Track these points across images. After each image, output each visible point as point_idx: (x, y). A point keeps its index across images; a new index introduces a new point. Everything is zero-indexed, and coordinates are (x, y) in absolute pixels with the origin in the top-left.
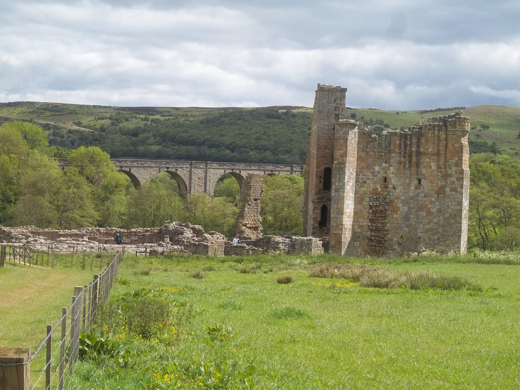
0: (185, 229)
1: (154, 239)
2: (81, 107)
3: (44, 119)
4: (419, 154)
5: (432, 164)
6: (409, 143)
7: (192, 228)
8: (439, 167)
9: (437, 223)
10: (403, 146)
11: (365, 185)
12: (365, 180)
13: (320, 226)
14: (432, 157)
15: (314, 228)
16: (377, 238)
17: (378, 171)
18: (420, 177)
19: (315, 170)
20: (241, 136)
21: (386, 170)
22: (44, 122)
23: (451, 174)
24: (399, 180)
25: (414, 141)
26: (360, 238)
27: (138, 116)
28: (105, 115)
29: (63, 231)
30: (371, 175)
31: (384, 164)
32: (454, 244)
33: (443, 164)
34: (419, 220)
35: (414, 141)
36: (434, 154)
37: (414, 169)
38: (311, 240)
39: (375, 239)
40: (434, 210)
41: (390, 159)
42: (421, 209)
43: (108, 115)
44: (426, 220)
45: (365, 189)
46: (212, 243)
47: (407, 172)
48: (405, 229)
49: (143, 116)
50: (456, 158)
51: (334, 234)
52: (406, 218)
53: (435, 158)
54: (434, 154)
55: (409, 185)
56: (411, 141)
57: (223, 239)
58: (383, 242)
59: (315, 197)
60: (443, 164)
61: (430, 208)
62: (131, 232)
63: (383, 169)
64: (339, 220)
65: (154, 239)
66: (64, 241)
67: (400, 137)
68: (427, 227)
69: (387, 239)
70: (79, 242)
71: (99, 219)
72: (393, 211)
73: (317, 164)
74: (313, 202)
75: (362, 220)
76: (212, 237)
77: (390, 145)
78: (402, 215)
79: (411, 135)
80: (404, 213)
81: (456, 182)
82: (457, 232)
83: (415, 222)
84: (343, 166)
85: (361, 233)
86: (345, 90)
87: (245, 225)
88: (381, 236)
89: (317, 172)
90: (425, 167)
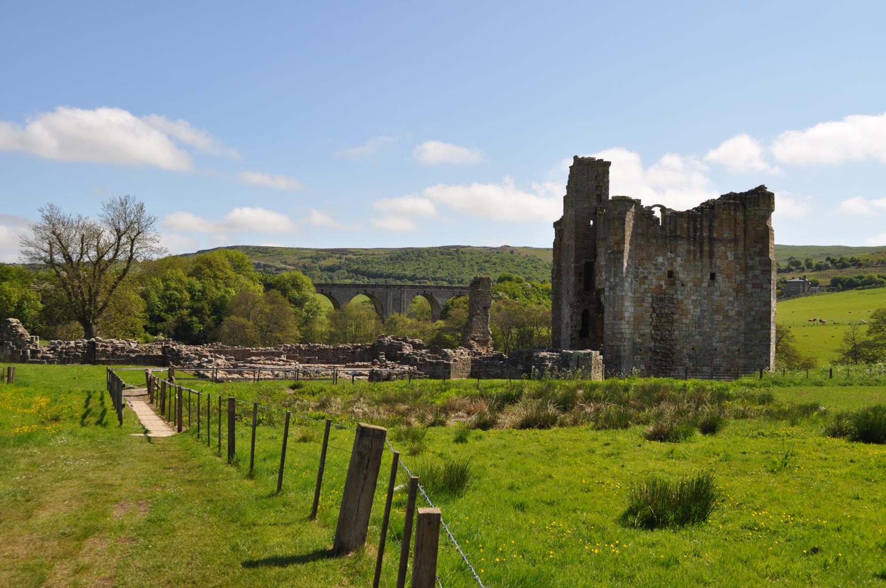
0: (404, 343)
1: (366, 357)
2: (287, 249)
3: (256, 259)
4: (712, 240)
5: (729, 254)
6: (699, 226)
7: (412, 343)
8: (736, 258)
9: (736, 330)
10: (691, 230)
11: (646, 282)
12: (646, 274)
13: (580, 336)
14: (728, 244)
15: (572, 339)
16: (663, 351)
17: (662, 263)
18: (714, 271)
19: (573, 265)
20: (421, 270)
21: (672, 261)
22: (257, 262)
23: (753, 266)
24: (688, 275)
25: (705, 223)
26: (641, 350)
27: (334, 255)
28: (306, 255)
29: (256, 350)
30: (654, 268)
31: (669, 254)
32: (760, 356)
33: (742, 254)
34: (715, 326)
35: (705, 223)
36: (730, 241)
37: (706, 260)
38: (590, 354)
39: (661, 352)
40: (732, 313)
41: (676, 247)
42: (716, 311)
43: (309, 255)
44: (723, 326)
45: (646, 286)
46: (455, 361)
47: (699, 264)
48: (697, 337)
49: (338, 255)
50: (760, 246)
51: (609, 346)
52: (698, 323)
53: (732, 245)
54: (730, 241)
55: (701, 280)
56: (701, 224)
57: (469, 355)
58: (671, 355)
59: (574, 300)
60: (742, 254)
61: (727, 311)
62: (339, 348)
63: (668, 259)
64: (616, 327)
65: (366, 357)
66: (255, 361)
67: (688, 218)
68: (724, 334)
69: (675, 352)
70: (274, 362)
71: (301, 337)
72: (682, 315)
73: (576, 257)
74: (571, 306)
75: (644, 327)
76: (455, 352)
77: (676, 229)
78: (693, 320)
79: (701, 217)
80: (695, 317)
81: (761, 277)
82: (765, 341)
83: (710, 328)
84: (620, 256)
85: (642, 344)
86: (609, 164)
87: (473, 339)
88: (668, 347)
89: (576, 267)
90: (720, 258)
